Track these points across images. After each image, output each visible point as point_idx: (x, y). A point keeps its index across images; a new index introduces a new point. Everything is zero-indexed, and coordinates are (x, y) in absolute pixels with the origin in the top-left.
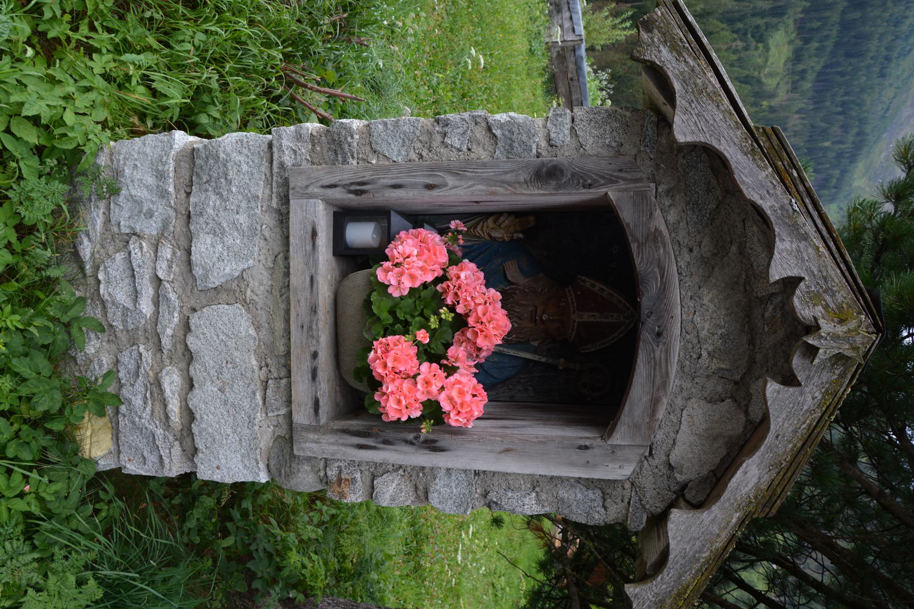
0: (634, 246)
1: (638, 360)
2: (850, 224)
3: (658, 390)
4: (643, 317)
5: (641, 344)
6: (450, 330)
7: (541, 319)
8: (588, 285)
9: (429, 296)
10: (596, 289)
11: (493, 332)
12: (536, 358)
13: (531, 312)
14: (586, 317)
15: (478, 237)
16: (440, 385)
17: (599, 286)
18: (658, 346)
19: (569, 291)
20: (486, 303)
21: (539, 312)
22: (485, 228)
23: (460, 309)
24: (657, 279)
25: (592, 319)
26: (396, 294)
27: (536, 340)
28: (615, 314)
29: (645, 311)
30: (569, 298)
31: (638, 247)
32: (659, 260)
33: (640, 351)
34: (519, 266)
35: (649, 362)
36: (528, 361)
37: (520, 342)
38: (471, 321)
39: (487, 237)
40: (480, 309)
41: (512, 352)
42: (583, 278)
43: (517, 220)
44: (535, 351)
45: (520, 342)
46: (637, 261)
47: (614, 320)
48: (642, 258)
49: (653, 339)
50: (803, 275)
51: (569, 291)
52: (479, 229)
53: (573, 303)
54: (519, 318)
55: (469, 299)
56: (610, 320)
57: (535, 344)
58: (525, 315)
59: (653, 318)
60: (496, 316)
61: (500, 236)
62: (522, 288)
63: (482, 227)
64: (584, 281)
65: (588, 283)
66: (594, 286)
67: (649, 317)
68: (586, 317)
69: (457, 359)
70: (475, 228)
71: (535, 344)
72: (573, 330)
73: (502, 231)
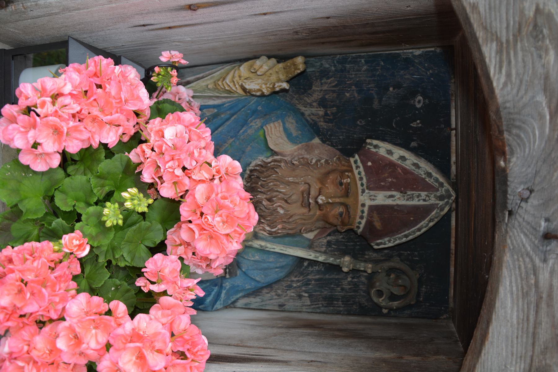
0: (489, 52)
1: (501, 290)
2: (15, 321)
3: (544, 352)
4: (512, 200)
5: (507, 258)
6: (159, 226)
7: (317, 202)
8: (382, 152)
9: (102, 167)
10: (394, 158)
11: (223, 230)
12: (311, 255)
13: (302, 193)
14: (381, 198)
15: (229, 92)
16: (103, 339)
17: (398, 153)
18: (545, 261)
19: (356, 162)
20: (212, 179)
21: (313, 192)
22: (237, 78)
23: (167, 191)
24: (542, 117)
25: (390, 202)
26: (39, 167)
27: (311, 231)
28: (423, 194)
29: (516, 187)
30: (356, 172)
31: (499, 52)
32: (547, 78)
33: (505, 272)
34: (285, 130)
35: (525, 295)
36: (302, 260)
37: (288, 235)
38: (184, 211)
39: (240, 91)
40: (200, 191)
41: (278, 248)
42: (375, 142)
43: (281, 65)
44: (310, 246)
45: (288, 235)
46: (498, 81)
47: (421, 203)
48: (509, 75)
49: (535, 248)
50: (24, 266)
51: (356, 162)
52: (228, 80)
53: (361, 179)
54: (286, 201)
55: (179, 172)
56: (415, 202)
57: (310, 236)
58: (293, 197)
59: (534, 201)
60: (227, 202)
61: (257, 87)
62: (288, 159)
63: (233, 77)
64: (376, 147)
65: (383, 149)
66: (390, 152)
67: (526, 200)
68: (381, 198)
69: (161, 280)
70: (224, 79)
71: (310, 236)
72: (362, 217)
73: (260, 81)
